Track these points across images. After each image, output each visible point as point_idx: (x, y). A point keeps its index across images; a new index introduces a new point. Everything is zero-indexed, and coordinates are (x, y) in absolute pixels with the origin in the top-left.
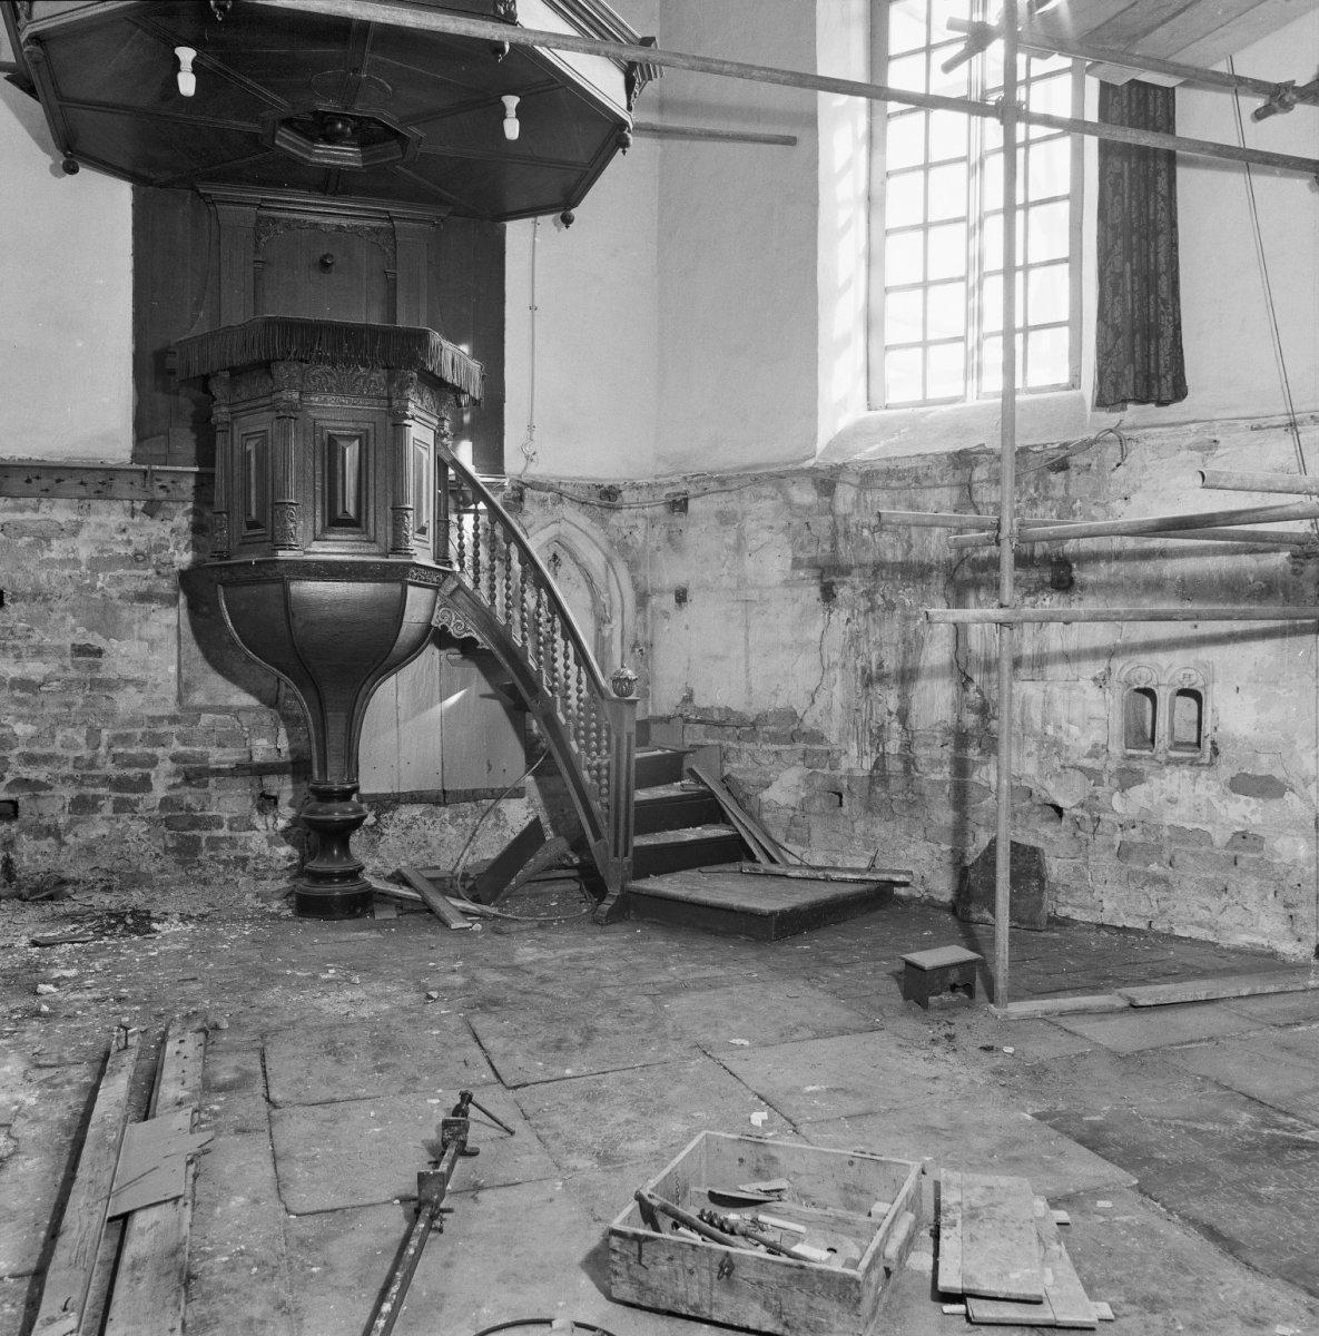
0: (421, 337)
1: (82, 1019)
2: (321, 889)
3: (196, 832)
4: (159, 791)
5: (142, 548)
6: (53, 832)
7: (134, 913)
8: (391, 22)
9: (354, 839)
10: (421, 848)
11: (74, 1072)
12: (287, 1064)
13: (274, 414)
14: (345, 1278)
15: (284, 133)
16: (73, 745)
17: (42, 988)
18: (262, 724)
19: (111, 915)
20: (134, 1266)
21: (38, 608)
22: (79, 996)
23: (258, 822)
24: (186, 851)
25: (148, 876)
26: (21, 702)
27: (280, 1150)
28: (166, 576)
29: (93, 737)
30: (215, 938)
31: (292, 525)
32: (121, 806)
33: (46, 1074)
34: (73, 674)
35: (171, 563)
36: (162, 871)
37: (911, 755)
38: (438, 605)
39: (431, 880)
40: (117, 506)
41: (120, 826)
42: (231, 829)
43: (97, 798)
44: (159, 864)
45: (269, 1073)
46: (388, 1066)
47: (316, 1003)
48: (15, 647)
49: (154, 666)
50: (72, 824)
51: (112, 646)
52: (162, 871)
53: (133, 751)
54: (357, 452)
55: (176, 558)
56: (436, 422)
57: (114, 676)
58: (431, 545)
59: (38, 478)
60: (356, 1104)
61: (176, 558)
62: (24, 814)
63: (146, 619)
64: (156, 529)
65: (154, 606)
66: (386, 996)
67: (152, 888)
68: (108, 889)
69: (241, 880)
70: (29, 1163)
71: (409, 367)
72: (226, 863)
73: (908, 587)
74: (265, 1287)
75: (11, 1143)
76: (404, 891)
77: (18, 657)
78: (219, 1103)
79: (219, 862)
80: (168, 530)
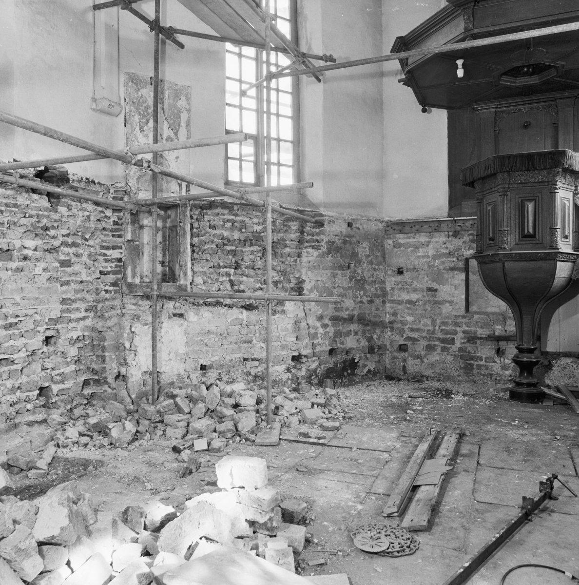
0: (563, 153)
1: (420, 423)
2: (519, 390)
3: (472, 362)
4: (458, 344)
5: (451, 250)
6: (419, 357)
7: (446, 390)
8: (528, 37)
9: (535, 369)
10: (571, 377)
11: (413, 440)
12: (488, 452)
13: (499, 194)
14: (489, 525)
15: (504, 78)
16: (427, 325)
17: (409, 411)
18: (499, 319)
19: (438, 390)
20: (418, 501)
21: (415, 274)
22: (421, 416)
23: (497, 359)
24: (468, 369)
25: (453, 378)
26: (409, 309)
27: (477, 480)
28: (461, 260)
29: (434, 322)
30: (474, 403)
31: (505, 239)
32: (444, 349)
33: (404, 439)
34: (427, 298)
35: (463, 255)
36: (459, 376)
37: (345, 341)
38: (575, 269)
39: (572, 392)
40: (443, 234)
41: (443, 357)
42: (486, 361)
43: (435, 345)
44: (458, 373)
45: (481, 453)
46: (529, 460)
47: (507, 433)
48: (407, 288)
49: (456, 296)
50: (426, 355)
51: (441, 288)
52: (459, 376)
53: (448, 328)
54: (533, 207)
55: (465, 253)
56: (574, 188)
57: (441, 299)
58: (571, 243)
59: (415, 226)
60: (512, 471)
61: (465, 253)
62: (410, 350)
63: (453, 277)
64: (457, 242)
65: (456, 272)
66: (537, 435)
67: (454, 382)
68: (439, 380)
69: (490, 383)
70: (394, 465)
71: (557, 167)
72: (484, 375)
73: (325, 326)
74: (460, 519)
75: (390, 457)
76: (558, 395)
77: (408, 292)
78: (460, 460)
79: (482, 375)
80: (461, 242)
